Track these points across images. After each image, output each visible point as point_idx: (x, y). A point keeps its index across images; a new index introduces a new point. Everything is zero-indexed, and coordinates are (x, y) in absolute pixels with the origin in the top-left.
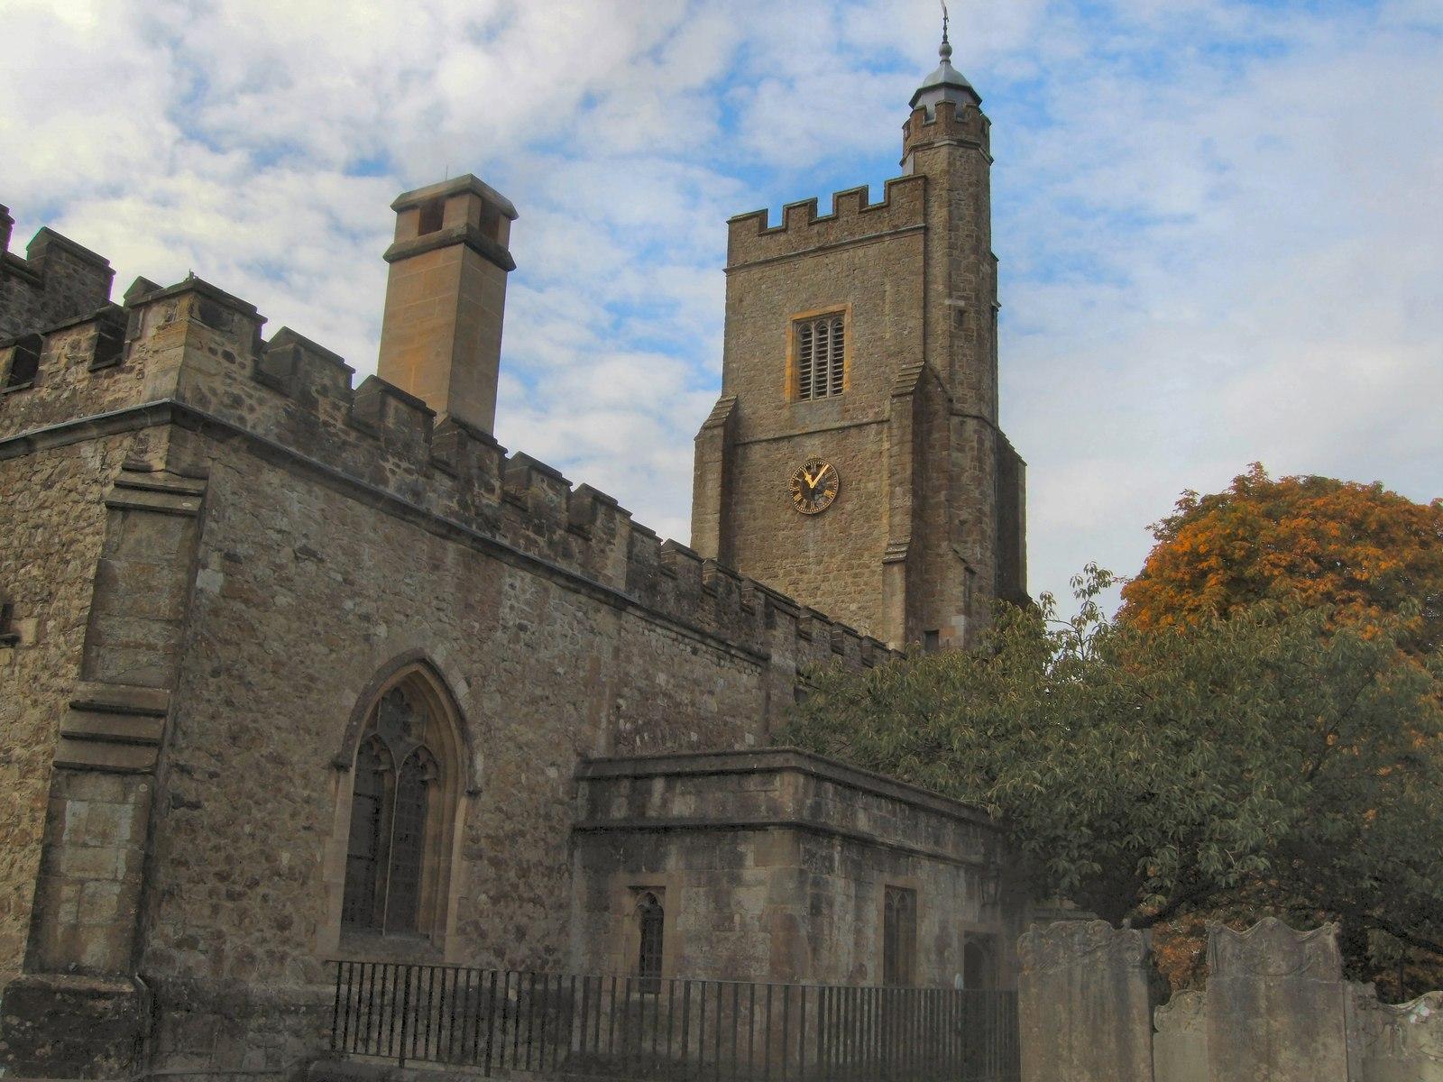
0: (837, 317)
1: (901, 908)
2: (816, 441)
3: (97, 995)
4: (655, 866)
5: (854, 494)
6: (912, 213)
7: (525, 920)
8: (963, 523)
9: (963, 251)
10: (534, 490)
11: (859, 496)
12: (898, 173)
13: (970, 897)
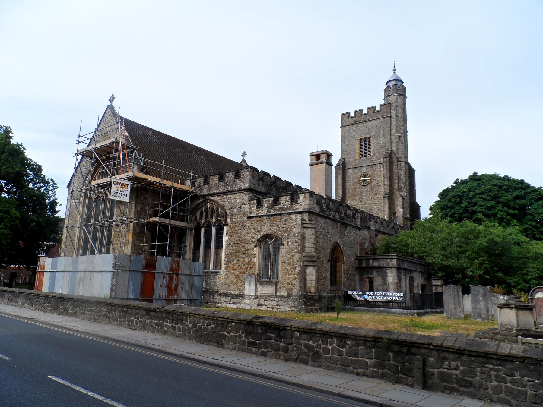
0: (369, 138)
1: (412, 279)
2: (365, 168)
3: (314, 296)
4: (372, 274)
5: (375, 181)
6: (387, 113)
8: (401, 187)
9: (400, 121)
10: (348, 212)
11: (376, 181)
12: (383, 102)
13: (422, 277)
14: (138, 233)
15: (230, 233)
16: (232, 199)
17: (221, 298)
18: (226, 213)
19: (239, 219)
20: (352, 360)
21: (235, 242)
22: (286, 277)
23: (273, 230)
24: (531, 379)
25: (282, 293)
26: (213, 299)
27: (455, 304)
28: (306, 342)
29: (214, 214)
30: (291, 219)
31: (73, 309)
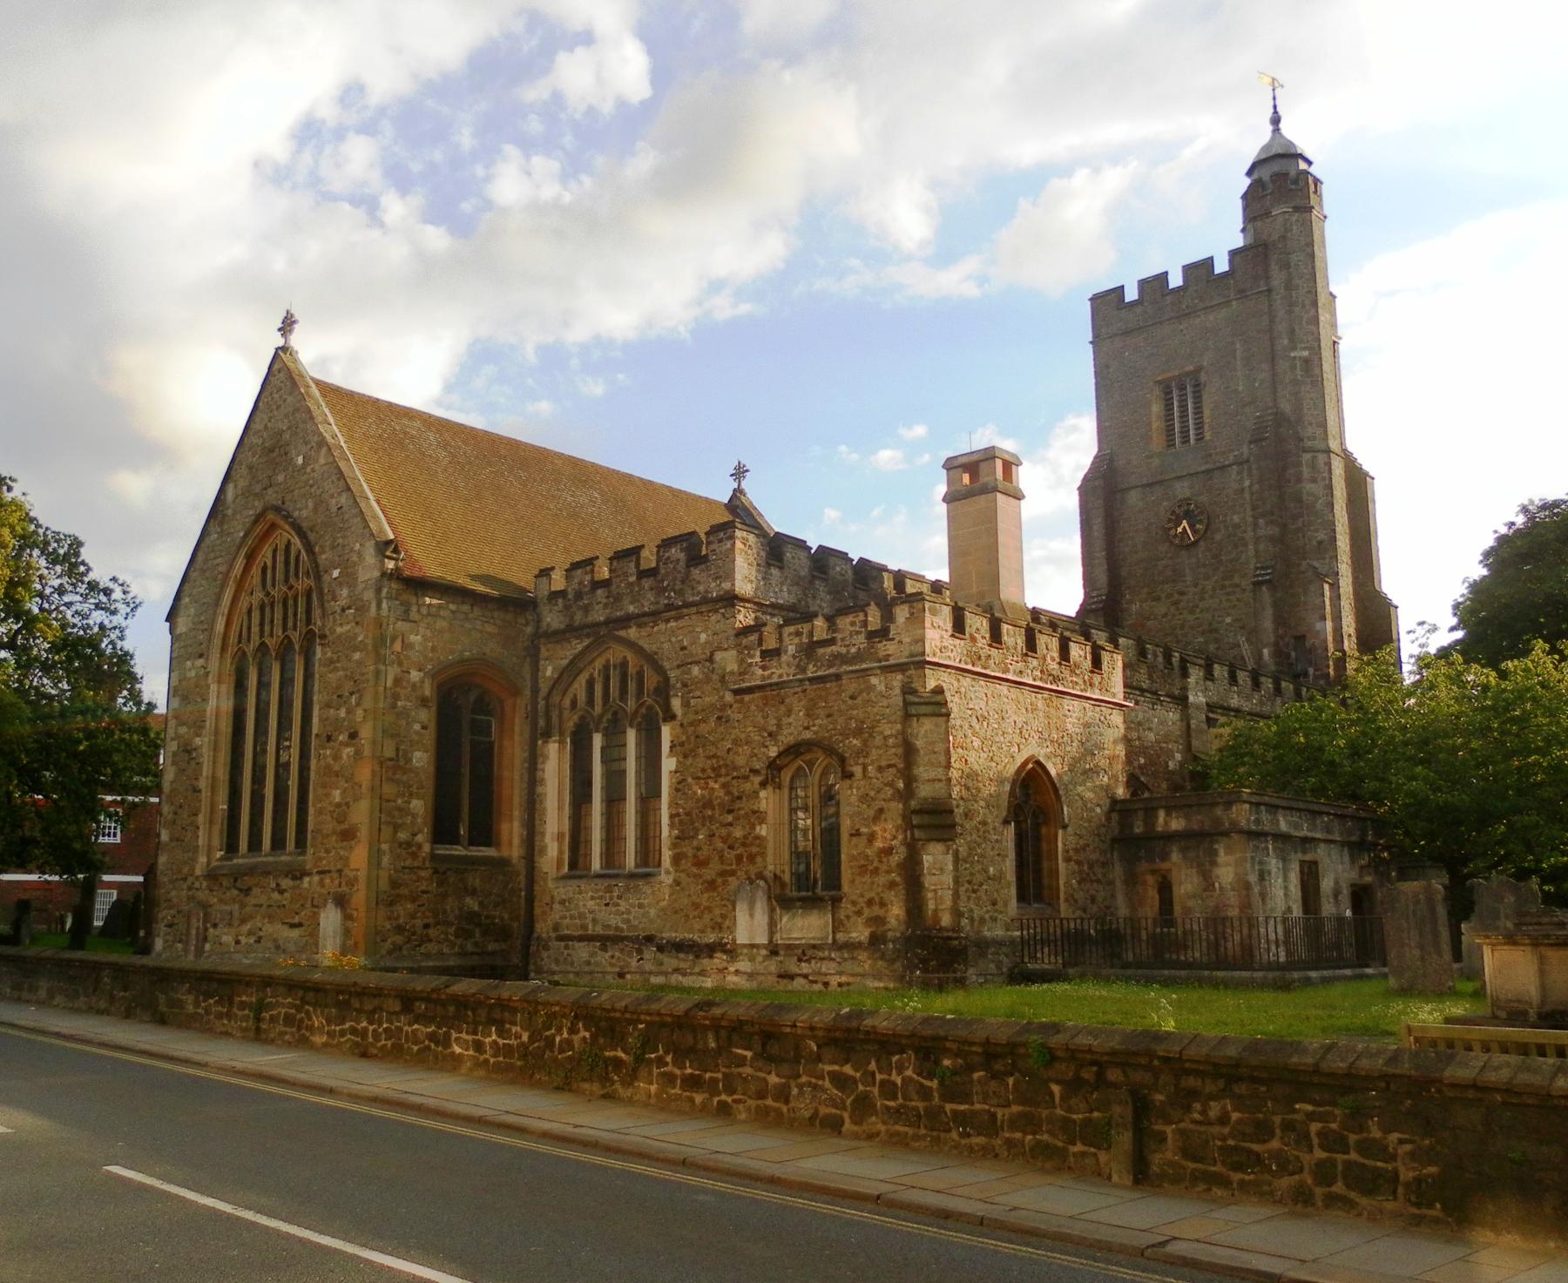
3: (950, 938)
4: (1165, 856)
7: (1094, 892)
8: (1320, 543)
9: (1304, 306)
11: (1226, 528)
12: (1238, 241)
14: (391, 759)
15: (682, 744)
16: (685, 635)
17: (665, 960)
18: (667, 679)
19: (707, 699)
20: (955, 1112)
21: (700, 775)
22: (864, 880)
23: (815, 729)
24: (1407, 1136)
25: (854, 935)
26: (639, 961)
27: (1422, 948)
28: (836, 1068)
29: (632, 686)
30: (871, 688)
31: (197, 1004)
